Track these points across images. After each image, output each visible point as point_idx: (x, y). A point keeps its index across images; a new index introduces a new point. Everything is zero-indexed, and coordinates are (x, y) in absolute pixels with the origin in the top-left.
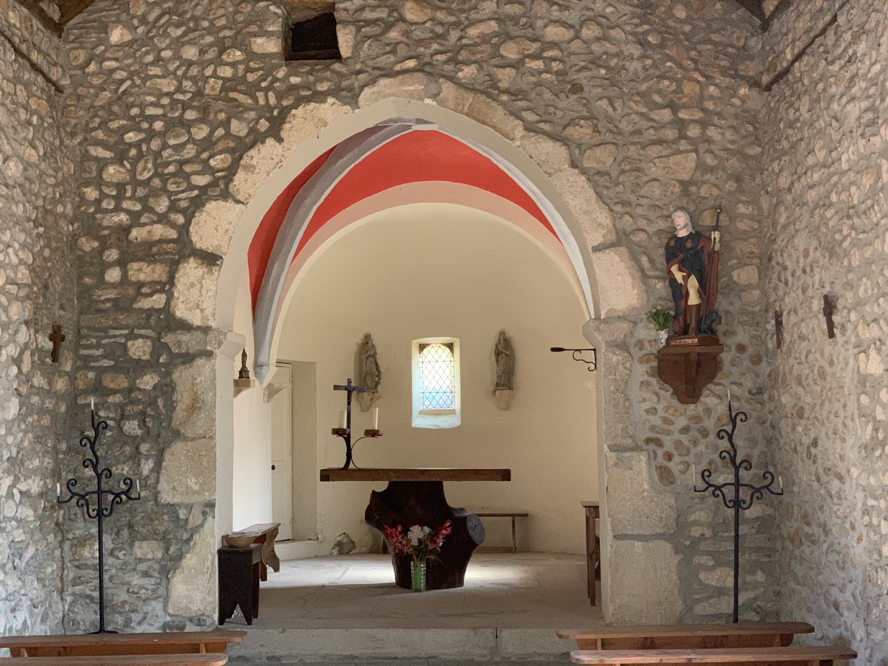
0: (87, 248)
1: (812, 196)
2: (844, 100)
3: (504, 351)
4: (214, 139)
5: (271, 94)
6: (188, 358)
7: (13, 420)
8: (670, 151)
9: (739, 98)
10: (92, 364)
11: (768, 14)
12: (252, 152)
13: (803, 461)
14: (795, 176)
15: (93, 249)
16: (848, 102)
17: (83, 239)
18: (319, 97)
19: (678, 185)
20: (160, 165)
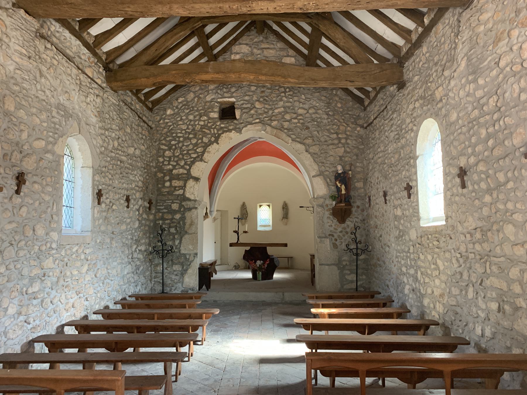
0: (160, 176)
1: (379, 160)
2: (390, 131)
3: (285, 207)
6: (190, 209)
12: (210, 147)
18: (230, 131)
20: (182, 151)
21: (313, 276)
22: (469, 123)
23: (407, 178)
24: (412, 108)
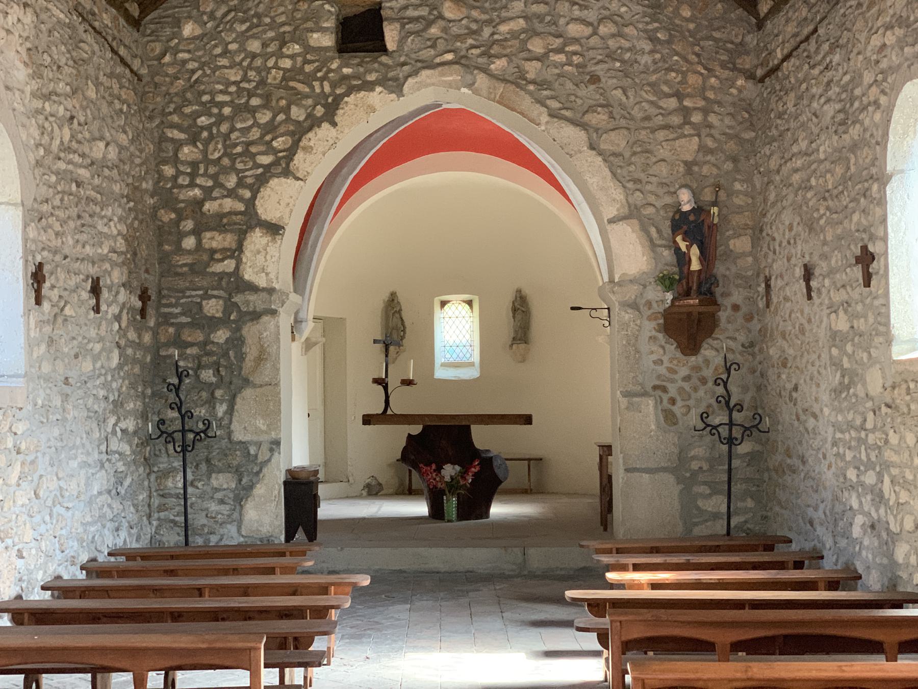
0: (166, 219)
1: (796, 178)
2: (823, 100)
3: (521, 307)
4: (276, 123)
5: (326, 83)
6: (255, 316)
7: (115, 369)
8: (675, 135)
9: (737, 89)
10: (172, 321)
11: (762, 15)
12: (310, 135)
13: (786, 403)
14: (783, 161)
15: (171, 219)
16: (825, 103)
17: (162, 211)
18: (369, 86)
19: (682, 165)
20: (229, 146)
21: (607, 506)
23: (864, 231)
24: (879, 44)
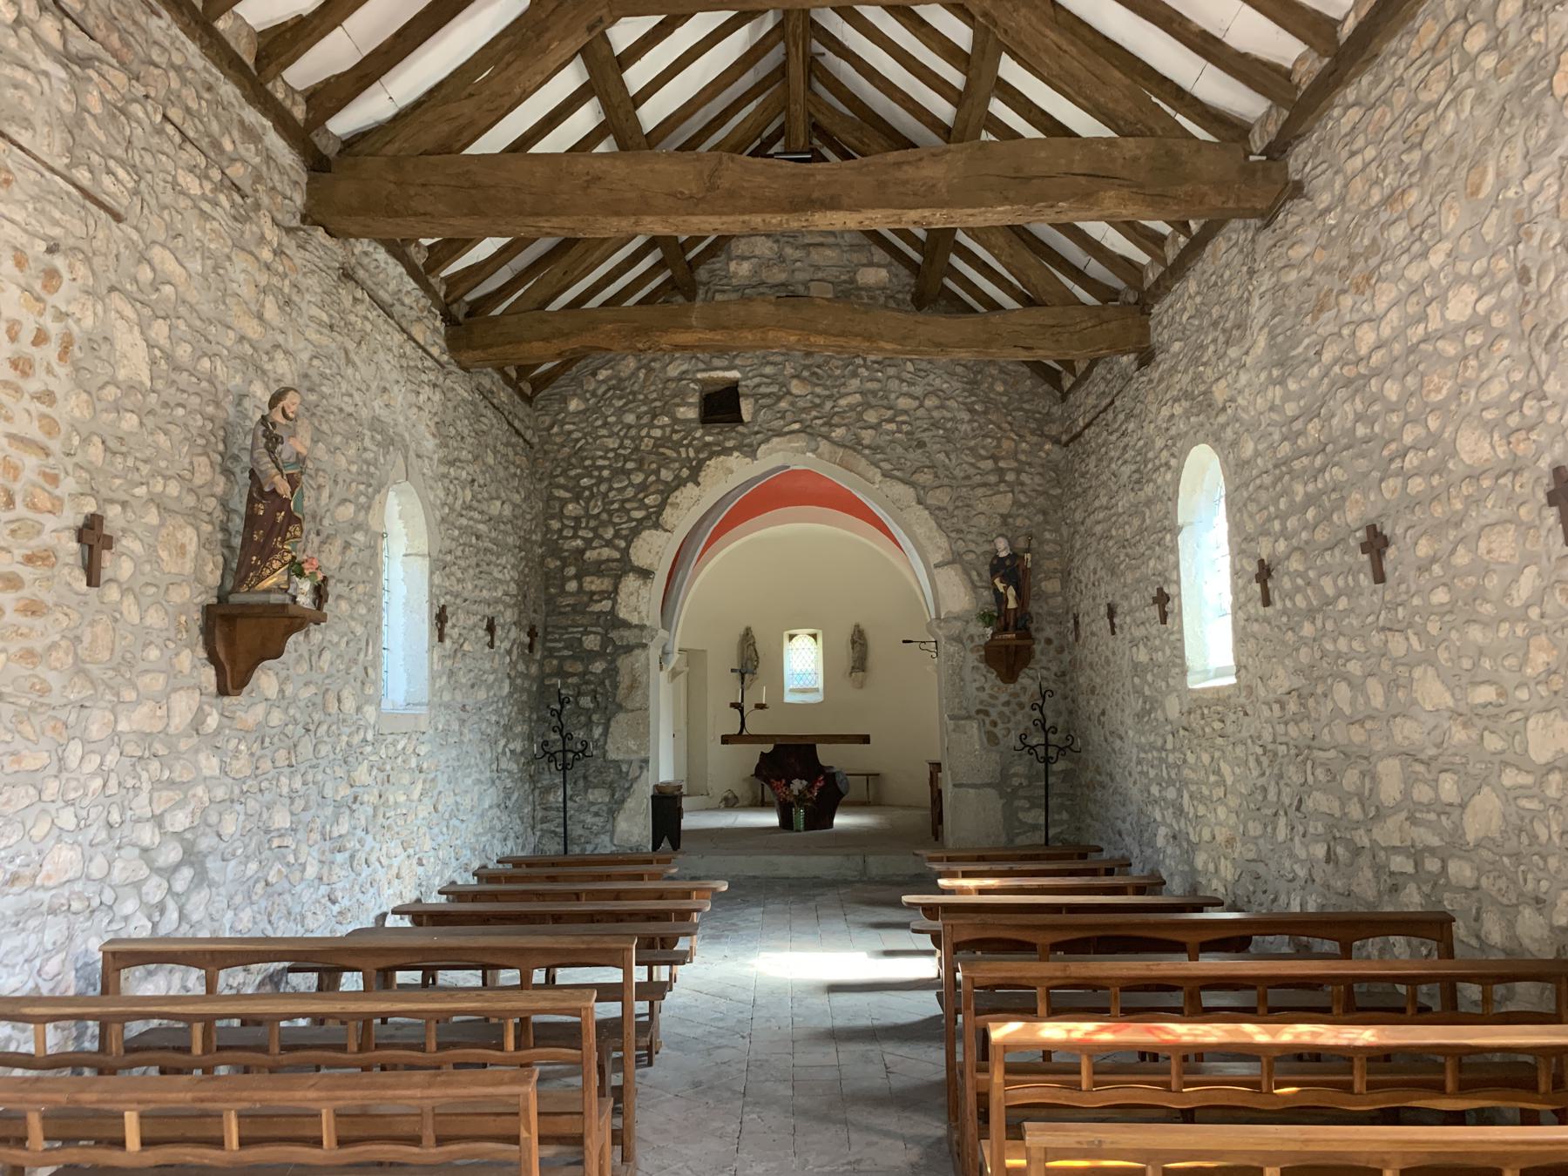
0: (552, 566)
1: (1098, 529)
6: (629, 649)
12: (677, 493)
18: (727, 452)
20: (607, 503)
22: (1276, 466)
